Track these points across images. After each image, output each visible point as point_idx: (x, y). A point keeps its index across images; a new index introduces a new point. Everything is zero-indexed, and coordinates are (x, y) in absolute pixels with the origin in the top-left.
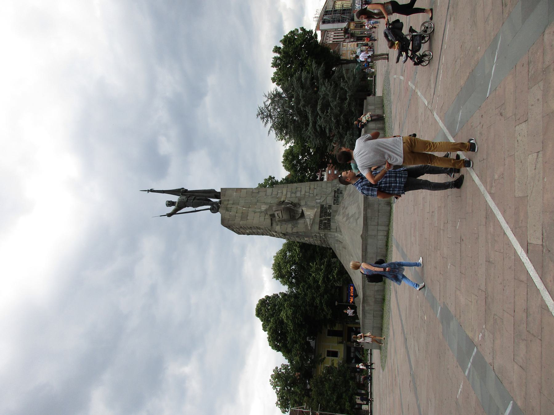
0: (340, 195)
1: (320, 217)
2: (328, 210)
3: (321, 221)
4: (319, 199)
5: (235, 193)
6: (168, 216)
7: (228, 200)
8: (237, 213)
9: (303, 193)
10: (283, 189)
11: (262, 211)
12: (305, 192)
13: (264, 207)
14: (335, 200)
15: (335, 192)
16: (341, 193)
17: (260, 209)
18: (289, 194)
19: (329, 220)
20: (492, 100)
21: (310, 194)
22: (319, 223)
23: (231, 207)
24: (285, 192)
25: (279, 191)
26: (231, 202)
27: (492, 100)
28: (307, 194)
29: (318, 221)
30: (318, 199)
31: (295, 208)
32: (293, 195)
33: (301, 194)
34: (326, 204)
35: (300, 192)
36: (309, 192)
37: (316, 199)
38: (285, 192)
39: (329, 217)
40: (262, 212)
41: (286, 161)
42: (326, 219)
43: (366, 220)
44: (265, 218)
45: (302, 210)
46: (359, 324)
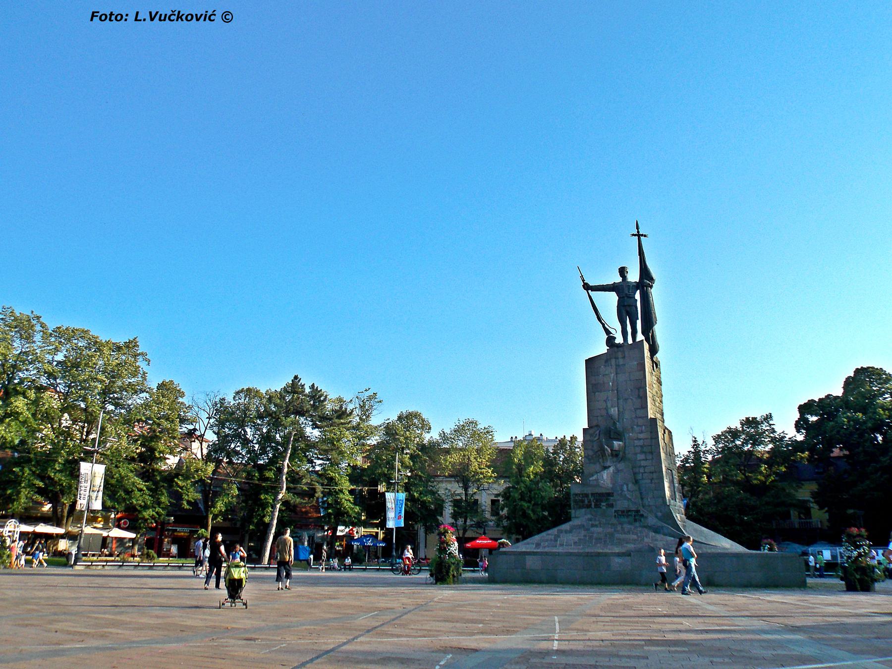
0: (631, 519)
1: (592, 494)
2: (605, 504)
3: (586, 495)
4: (628, 490)
5: (636, 363)
6: (583, 286)
7: (624, 357)
8: (604, 375)
9: (643, 463)
10: (649, 433)
11: (609, 410)
12: (645, 467)
13: (614, 411)
14: (623, 512)
15: (638, 511)
16: (635, 520)
17: (612, 407)
18: (641, 443)
19: (589, 506)
20: (103, 403)
21: (641, 474)
22: (582, 492)
23: (611, 365)
24: (641, 436)
25: (644, 427)
26: (621, 361)
27: (103, 403)
28: (642, 470)
29: (585, 492)
30: (627, 488)
31: (609, 456)
32: (638, 450)
33: (640, 460)
34: (615, 500)
35: (644, 458)
36: (645, 472)
37: (627, 485)
38: (641, 436)
39: (593, 506)
40: (607, 410)
41: (623, 428)
42: (590, 501)
43: (577, 555)
44: (597, 417)
45: (610, 467)
46: (287, 489)
